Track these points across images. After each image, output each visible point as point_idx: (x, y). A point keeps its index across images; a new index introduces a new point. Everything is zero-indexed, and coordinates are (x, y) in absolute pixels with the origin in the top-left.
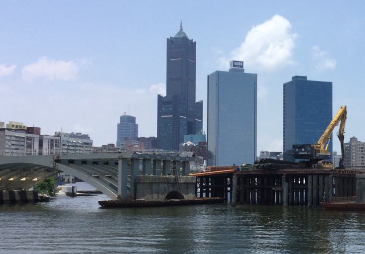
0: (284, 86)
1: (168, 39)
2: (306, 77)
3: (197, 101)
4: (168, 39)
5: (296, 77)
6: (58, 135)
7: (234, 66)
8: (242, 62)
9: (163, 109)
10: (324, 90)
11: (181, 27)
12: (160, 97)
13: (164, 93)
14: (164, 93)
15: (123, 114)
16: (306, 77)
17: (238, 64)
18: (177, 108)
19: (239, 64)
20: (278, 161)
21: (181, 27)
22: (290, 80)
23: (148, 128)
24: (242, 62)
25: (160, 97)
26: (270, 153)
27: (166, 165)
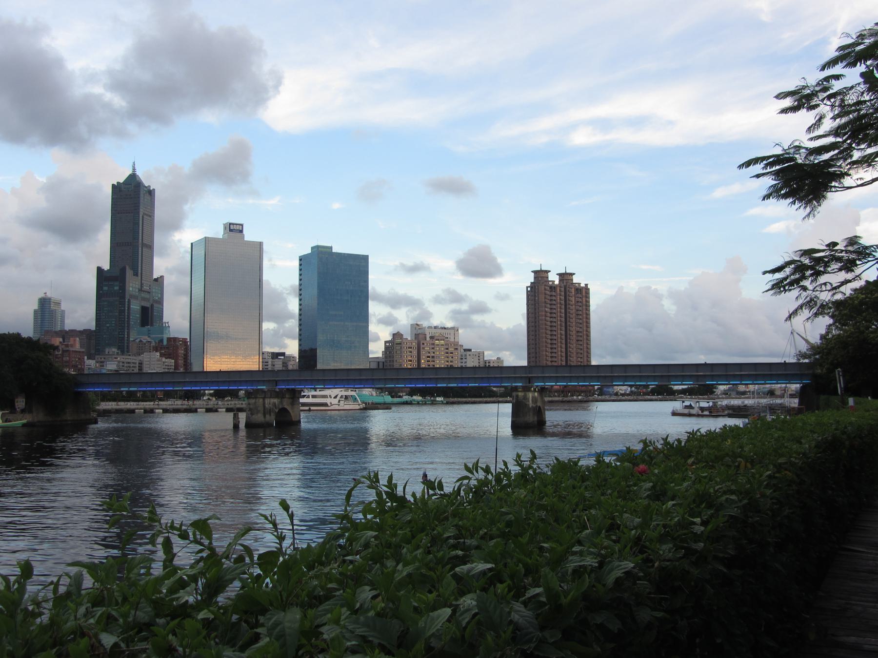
0: (300, 260)
1: (113, 185)
2: (331, 248)
3: (155, 277)
4: (113, 185)
5: (318, 247)
6: (279, 92)
7: (231, 230)
8: (242, 225)
9: (105, 288)
10: (358, 266)
11: (134, 169)
12: (100, 270)
13: (106, 266)
14: (106, 266)
15: (43, 295)
16: (331, 248)
17: (235, 227)
18: (125, 280)
19: (238, 227)
20: (286, 371)
21: (134, 169)
22: (309, 251)
23: (81, 314)
24: (242, 225)
25: (100, 270)
26: (366, 431)
27: (98, 250)
